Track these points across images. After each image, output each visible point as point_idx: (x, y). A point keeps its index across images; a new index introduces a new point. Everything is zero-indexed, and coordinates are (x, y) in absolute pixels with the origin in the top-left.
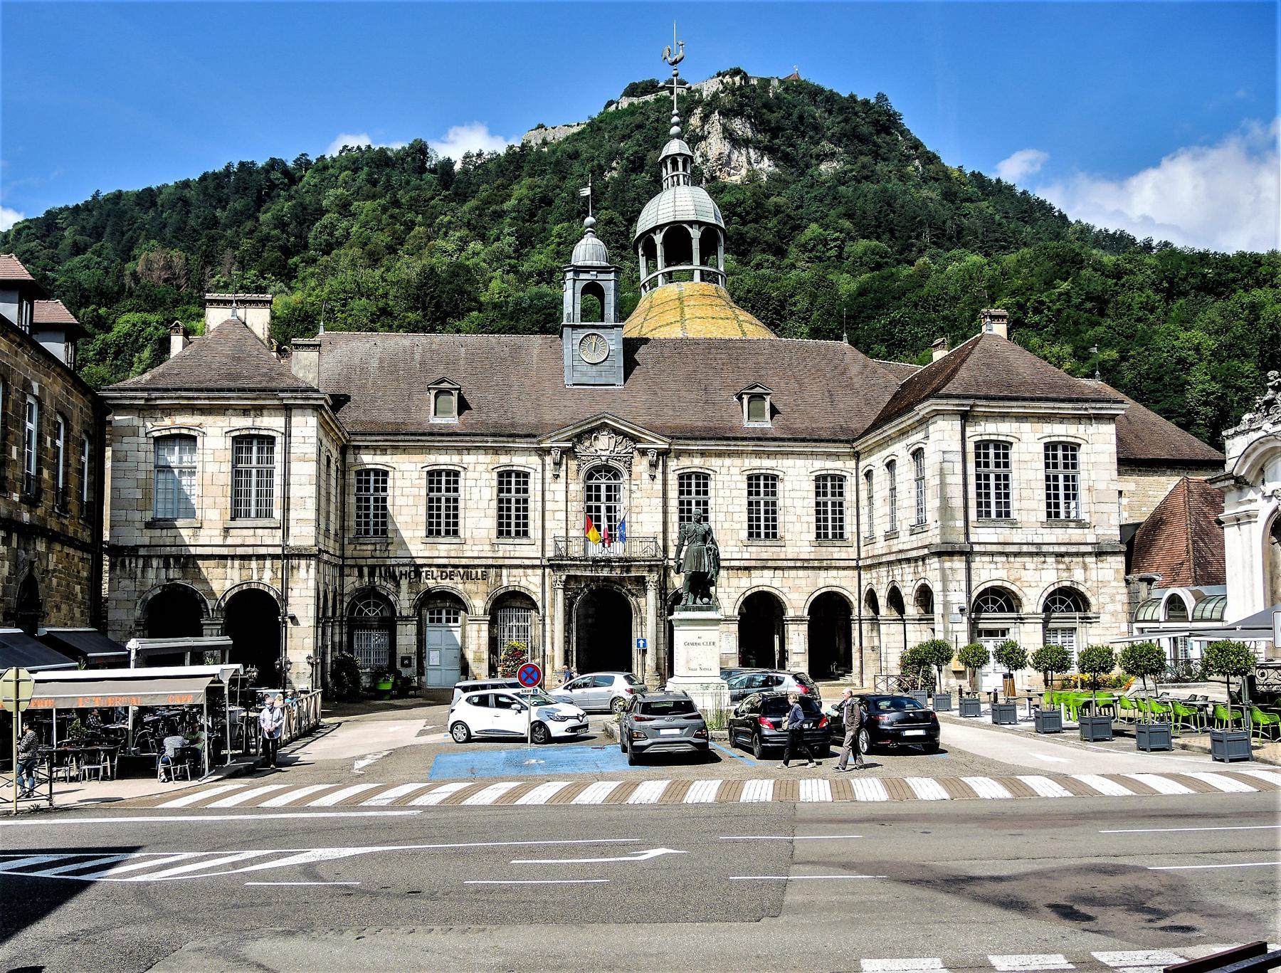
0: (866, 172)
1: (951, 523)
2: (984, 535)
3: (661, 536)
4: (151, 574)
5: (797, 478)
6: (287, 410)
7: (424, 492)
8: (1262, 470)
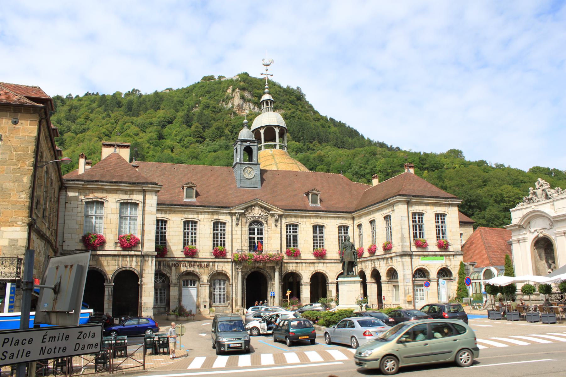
0: (293, 115)
1: (405, 244)
5: (331, 227)
6: (144, 192)
7: (182, 230)
8: (529, 223)
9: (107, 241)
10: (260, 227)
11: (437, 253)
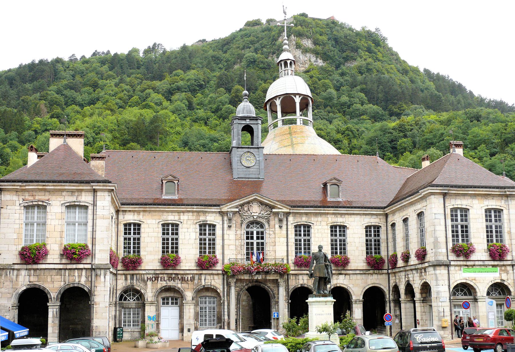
1: (440, 250)
3: (285, 258)
4: (21, 278)
9: (51, 252)
10: (260, 230)
11: (487, 263)
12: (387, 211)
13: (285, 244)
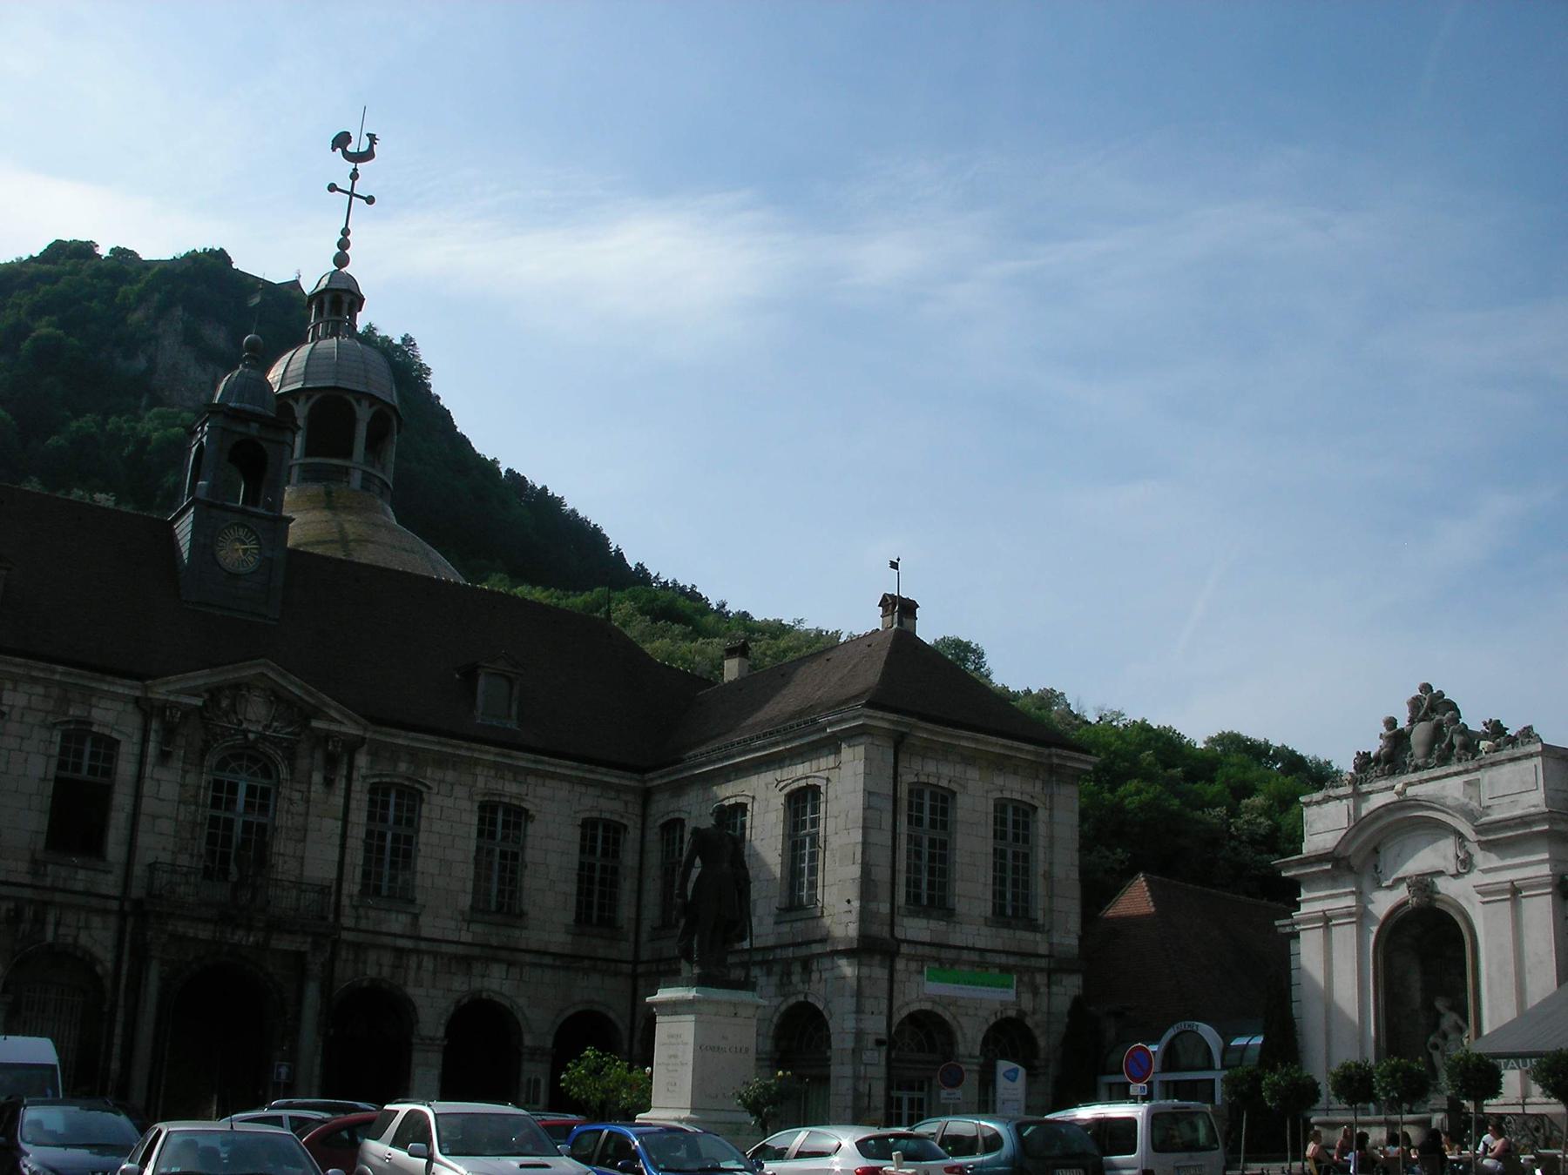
1: (873, 906)
2: (916, 928)
8: (1376, 851)
10: (260, 782)
12: (655, 779)
13: (337, 840)
